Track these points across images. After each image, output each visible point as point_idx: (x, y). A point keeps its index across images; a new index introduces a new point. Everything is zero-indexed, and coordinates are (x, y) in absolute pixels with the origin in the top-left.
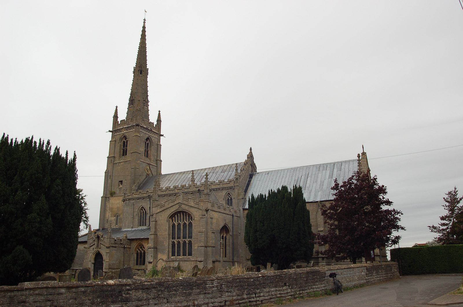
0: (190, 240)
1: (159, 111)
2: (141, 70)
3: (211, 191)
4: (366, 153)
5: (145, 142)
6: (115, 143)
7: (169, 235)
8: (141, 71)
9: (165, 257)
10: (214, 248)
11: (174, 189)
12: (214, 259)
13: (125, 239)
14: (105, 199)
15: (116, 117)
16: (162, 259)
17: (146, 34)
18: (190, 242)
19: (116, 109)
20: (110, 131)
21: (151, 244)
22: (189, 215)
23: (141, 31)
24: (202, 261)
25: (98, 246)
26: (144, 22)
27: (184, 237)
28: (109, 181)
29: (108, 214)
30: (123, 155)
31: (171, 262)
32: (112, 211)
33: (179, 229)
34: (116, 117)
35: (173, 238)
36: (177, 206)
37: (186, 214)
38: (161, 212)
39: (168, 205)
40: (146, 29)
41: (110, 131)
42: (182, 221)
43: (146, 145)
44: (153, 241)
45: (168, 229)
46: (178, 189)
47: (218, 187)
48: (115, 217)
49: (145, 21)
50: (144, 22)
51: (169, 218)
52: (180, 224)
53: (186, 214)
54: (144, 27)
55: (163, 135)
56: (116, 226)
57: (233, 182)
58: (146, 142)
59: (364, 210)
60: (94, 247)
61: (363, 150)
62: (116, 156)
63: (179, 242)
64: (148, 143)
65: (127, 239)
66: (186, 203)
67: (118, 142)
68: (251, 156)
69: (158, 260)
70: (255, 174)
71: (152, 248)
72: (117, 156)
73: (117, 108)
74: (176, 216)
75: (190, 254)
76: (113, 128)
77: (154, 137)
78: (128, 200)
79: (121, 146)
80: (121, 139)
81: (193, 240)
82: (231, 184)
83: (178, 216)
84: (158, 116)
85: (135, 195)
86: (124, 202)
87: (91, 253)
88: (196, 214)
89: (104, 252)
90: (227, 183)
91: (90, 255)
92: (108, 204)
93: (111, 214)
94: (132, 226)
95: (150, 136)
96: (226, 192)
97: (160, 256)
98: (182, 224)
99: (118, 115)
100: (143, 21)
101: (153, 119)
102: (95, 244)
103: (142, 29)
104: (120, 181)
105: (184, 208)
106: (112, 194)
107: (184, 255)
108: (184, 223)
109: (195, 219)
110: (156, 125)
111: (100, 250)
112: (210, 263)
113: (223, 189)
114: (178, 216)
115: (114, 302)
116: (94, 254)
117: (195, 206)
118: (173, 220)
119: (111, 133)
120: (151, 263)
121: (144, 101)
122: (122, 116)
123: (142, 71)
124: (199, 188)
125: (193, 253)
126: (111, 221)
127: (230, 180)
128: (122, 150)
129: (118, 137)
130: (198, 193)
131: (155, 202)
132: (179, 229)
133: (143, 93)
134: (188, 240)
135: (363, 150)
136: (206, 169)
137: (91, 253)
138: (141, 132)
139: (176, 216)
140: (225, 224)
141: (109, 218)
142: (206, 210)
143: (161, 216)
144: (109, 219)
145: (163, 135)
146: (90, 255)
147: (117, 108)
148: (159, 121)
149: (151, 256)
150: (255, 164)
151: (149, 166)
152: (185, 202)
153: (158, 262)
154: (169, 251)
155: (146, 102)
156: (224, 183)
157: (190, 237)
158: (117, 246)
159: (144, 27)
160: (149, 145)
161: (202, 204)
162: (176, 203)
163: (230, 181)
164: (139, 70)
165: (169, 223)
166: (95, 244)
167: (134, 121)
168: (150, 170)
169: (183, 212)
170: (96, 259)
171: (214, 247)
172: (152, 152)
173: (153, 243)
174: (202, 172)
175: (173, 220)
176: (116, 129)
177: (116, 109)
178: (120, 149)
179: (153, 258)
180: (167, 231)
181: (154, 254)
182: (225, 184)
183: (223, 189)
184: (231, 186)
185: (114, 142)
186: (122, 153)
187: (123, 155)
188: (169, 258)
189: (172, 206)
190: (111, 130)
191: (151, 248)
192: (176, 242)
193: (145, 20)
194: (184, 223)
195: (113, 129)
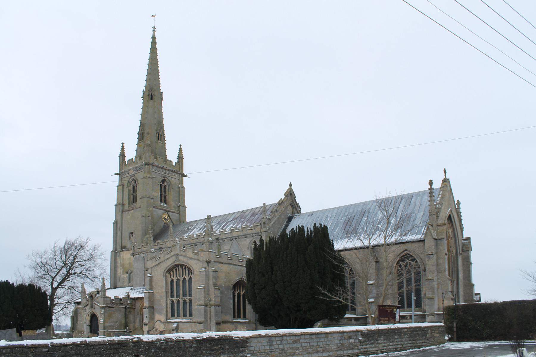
0: (184, 298)
1: (180, 146)
2: (151, 94)
3: (232, 239)
4: (449, 179)
5: (159, 186)
6: (123, 188)
7: (166, 292)
8: (152, 96)
9: (163, 319)
10: (220, 308)
11: (188, 239)
12: (220, 320)
13: (127, 298)
14: (115, 254)
15: (122, 156)
16: (160, 320)
17: (157, 46)
18: (191, 301)
19: (123, 147)
20: (116, 174)
21: (146, 304)
22: (189, 269)
23: (157, 43)
24: (202, 323)
25: (92, 307)
26: (154, 31)
27: (178, 296)
28: (119, 234)
29: (120, 271)
30: (133, 202)
31: (169, 324)
32: (123, 268)
33: (178, 285)
34: (122, 156)
35: (172, 296)
36: (174, 258)
37: (185, 267)
38: (157, 265)
39: (164, 257)
40: (157, 41)
41: (116, 174)
42: (179, 276)
43: (163, 188)
44: (148, 300)
45: (165, 286)
46: (193, 239)
47: (241, 234)
48: (127, 274)
49: (155, 30)
50: (154, 31)
51: (166, 273)
52: (179, 279)
53: (185, 267)
54: (154, 38)
55: (186, 176)
56: (129, 284)
57: (259, 227)
58: (161, 185)
59: (184, 237)
60: (88, 307)
61: (445, 176)
62: (124, 202)
63: (178, 302)
64: (165, 187)
65: (129, 298)
66: (184, 254)
67: (125, 186)
68: (290, 194)
69: (155, 322)
70: (296, 216)
71: (147, 308)
72: (126, 202)
73: (123, 145)
74: (174, 270)
75: (191, 315)
76: (119, 170)
77: (173, 179)
78: (137, 254)
79: (130, 192)
80: (129, 182)
81: (193, 298)
82: (256, 229)
83: (176, 270)
84: (179, 151)
85: (145, 247)
86: (133, 256)
87: (85, 314)
88: (196, 266)
89: (99, 313)
90: (252, 228)
91: (84, 316)
92: (118, 260)
93: (123, 271)
94: (143, 283)
95: (167, 177)
96: (251, 240)
97: (157, 317)
98: (181, 279)
99: (125, 154)
100: (153, 29)
101: (172, 156)
102: (88, 304)
103: (151, 40)
104: (131, 233)
105: (183, 260)
106: (123, 248)
107: (185, 315)
108: (171, 280)
109: (195, 273)
110: (175, 163)
111: (94, 311)
112: (213, 325)
113: (245, 236)
114: (176, 270)
115: (224, 353)
116: (88, 315)
117: (194, 258)
118: (171, 275)
119: (118, 176)
120: (146, 325)
121: (157, 133)
122: (131, 154)
123: (153, 95)
124: (218, 236)
125: (194, 313)
126: (123, 279)
127: (255, 225)
128: (132, 196)
129: (125, 181)
130: (216, 242)
131: (150, 254)
132: (178, 285)
133: (156, 124)
134: (188, 298)
135: (445, 176)
136: (233, 213)
137: (85, 314)
138: (153, 173)
139: (174, 270)
140: (241, 278)
141: (121, 276)
142: (206, 261)
143: (157, 270)
144: (122, 277)
145: (186, 176)
146: (84, 316)
147: (123, 145)
148: (180, 158)
149: (147, 317)
150: (297, 204)
151: (168, 213)
152: (182, 253)
153: (156, 324)
154: (167, 311)
155: (160, 135)
156: (248, 229)
157: (190, 295)
158: (115, 306)
159: (154, 38)
160: (167, 188)
161: (202, 254)
162: (172, 254)
163: (255, 226)
164: (149, 95)
165: (166, 278)
166: (88, 304)
167: (143, 159)
168: (170, 218)
169: (182, 266)
170: (91, 321)
171: (218, 306)
172: (171, 197)
173: (148, 302)
174: (229, 217)
175: (171, 275)
176: (123, 171)
177: (123, 147)
178: (129, 195)
179: (149, 319)
180: (164, 289)
181: (149, 315)
182: (249, 230)
183: (245, 236)
184: (257, 232)
185: (122, 187)
186: (132, 200)
187: (133, 202)
188: (167, 319)
189: (168, 258)
190: (118, 172)
191: (145, 308)
192: (175, 300)
193: (154, 28)
194: (177, 280)
195: (119, 171)
